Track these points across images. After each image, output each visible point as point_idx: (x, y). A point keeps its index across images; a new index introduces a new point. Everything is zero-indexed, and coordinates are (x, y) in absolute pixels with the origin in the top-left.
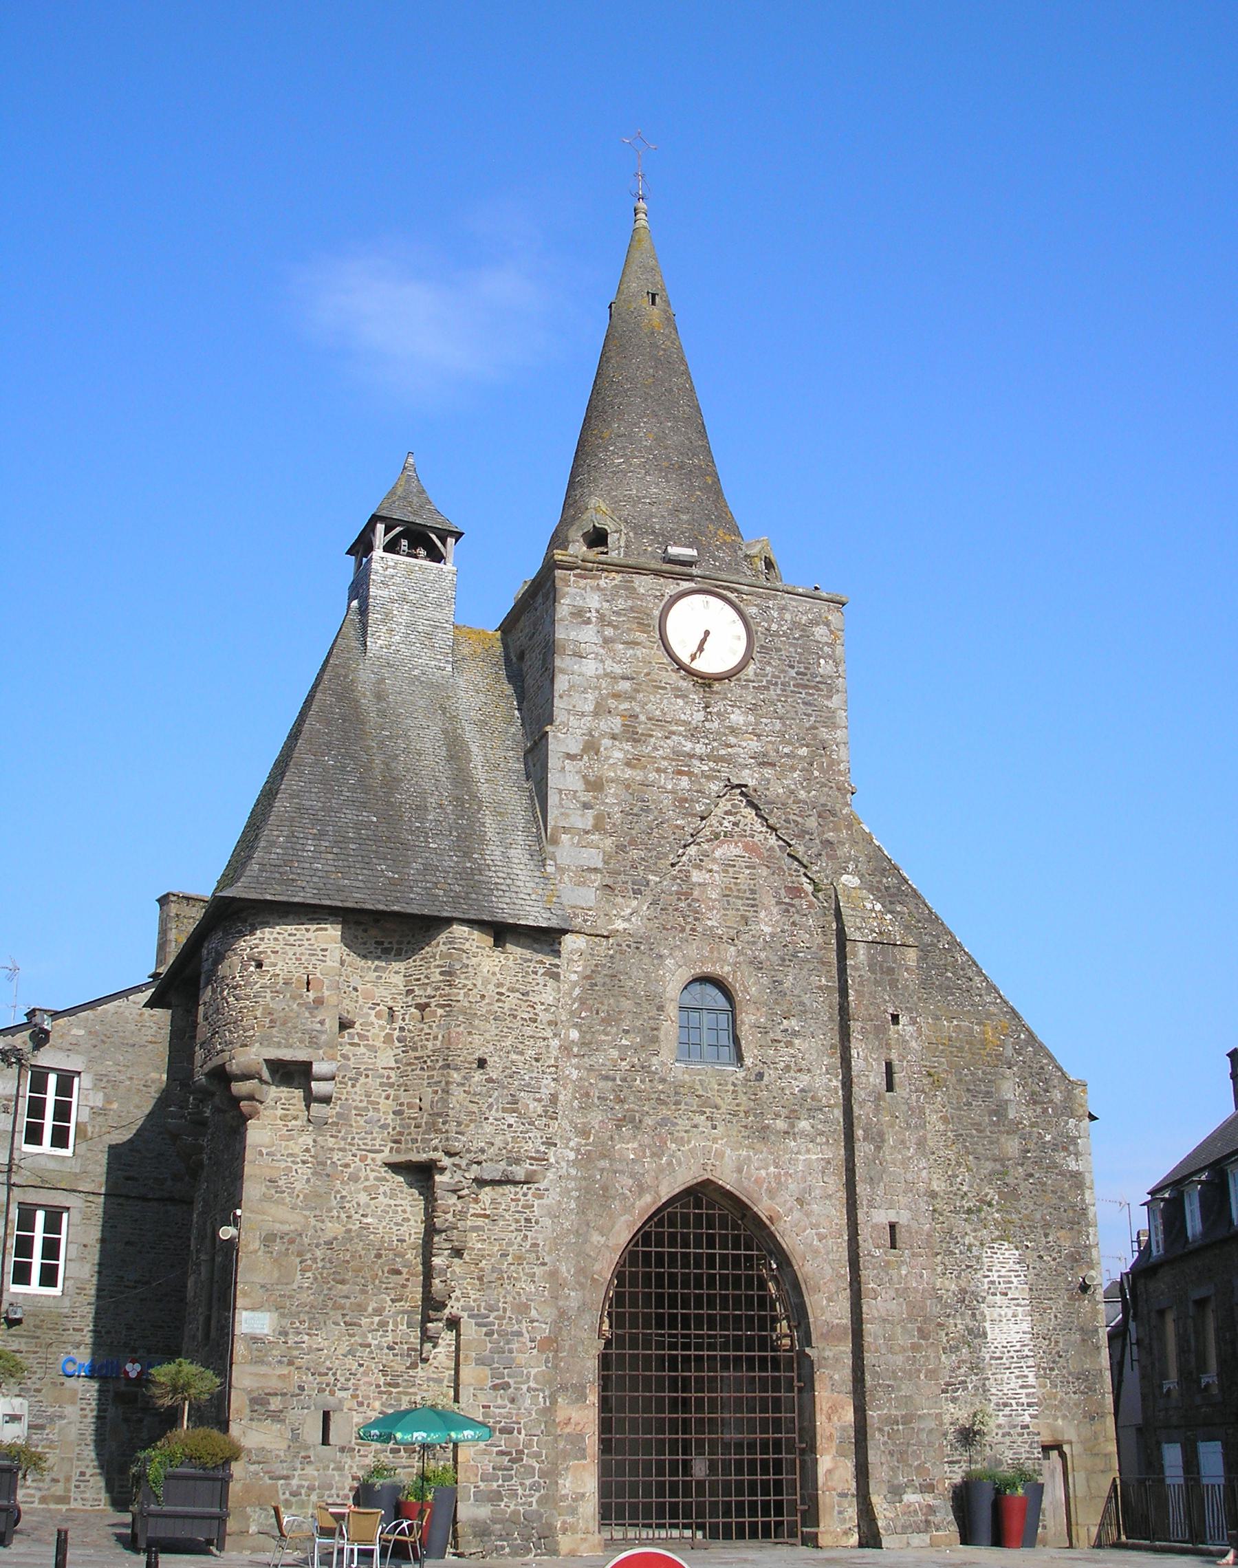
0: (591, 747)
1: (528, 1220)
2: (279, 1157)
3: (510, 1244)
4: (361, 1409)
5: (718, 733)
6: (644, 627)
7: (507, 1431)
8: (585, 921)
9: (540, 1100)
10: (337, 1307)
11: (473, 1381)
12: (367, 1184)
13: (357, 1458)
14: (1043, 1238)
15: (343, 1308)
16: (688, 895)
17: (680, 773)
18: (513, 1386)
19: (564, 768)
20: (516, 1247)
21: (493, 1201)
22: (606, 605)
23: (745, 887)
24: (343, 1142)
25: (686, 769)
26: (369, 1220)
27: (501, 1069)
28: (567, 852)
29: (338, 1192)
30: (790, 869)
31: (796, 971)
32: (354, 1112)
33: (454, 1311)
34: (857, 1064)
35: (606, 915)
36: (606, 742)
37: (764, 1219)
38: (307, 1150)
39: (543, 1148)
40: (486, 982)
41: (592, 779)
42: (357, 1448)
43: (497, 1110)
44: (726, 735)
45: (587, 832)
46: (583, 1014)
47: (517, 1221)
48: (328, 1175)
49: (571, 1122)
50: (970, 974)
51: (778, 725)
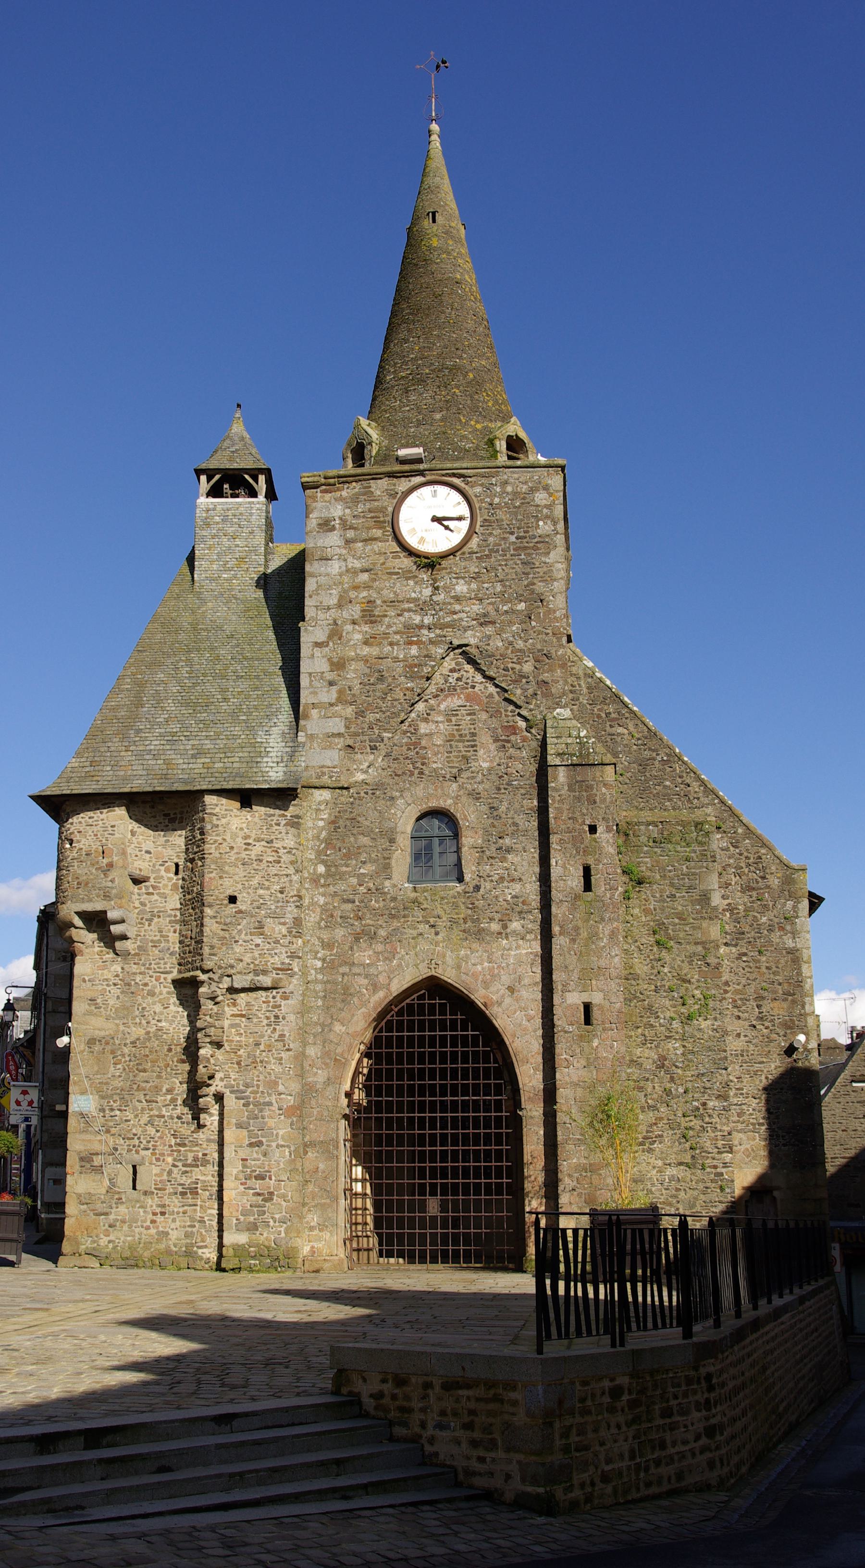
0: (335, 633)
1: (277, 1017)
2: (98, 982)
3: (262, 1036)
4: (159, 1163)
5: (444, 604)
6: (379, 524)
7: (260, 1177)
8: (331, 777)
9: (284, 924)
10: (139, 1089)
11: (234, 1141)
12: (161, 997)
13: (156, 1199)
14: (757, 1010)
15: (145, 1090)
16: (416, 744)
17: (411, 643)
18: (265, 1143)
19: (313, 655)
20: (266, 1038)
21: (248, 1004)
22: (348, 511)
23: (467, 732)
24: (143, 968)
25: (415, 639)
26: (163, 1024)
27: (249, 902)
28: (313, 724)
29: (139, 1005)
30: (506, 711)
31: (510, 797)
32: (150, 944)
33: (219, 1089)
34: (556, 871)
35: (348, 770)
36: (349, 627)
37: (480, 1004)
38: (117, 976)
39: (287, 961)
40: (234, 836)
41: (335, 660)
42: (156, 1191)
43: (246, 934)
44: (450, 604)
45: (331, 705)
46: (328, 852)
47: (268, 1018)
48: (132, 993)
49: (319, 938)
50: (688, 781)
51: (499, 588)
